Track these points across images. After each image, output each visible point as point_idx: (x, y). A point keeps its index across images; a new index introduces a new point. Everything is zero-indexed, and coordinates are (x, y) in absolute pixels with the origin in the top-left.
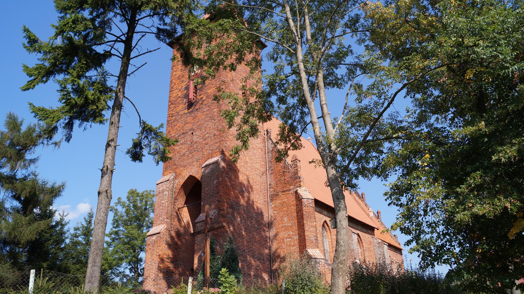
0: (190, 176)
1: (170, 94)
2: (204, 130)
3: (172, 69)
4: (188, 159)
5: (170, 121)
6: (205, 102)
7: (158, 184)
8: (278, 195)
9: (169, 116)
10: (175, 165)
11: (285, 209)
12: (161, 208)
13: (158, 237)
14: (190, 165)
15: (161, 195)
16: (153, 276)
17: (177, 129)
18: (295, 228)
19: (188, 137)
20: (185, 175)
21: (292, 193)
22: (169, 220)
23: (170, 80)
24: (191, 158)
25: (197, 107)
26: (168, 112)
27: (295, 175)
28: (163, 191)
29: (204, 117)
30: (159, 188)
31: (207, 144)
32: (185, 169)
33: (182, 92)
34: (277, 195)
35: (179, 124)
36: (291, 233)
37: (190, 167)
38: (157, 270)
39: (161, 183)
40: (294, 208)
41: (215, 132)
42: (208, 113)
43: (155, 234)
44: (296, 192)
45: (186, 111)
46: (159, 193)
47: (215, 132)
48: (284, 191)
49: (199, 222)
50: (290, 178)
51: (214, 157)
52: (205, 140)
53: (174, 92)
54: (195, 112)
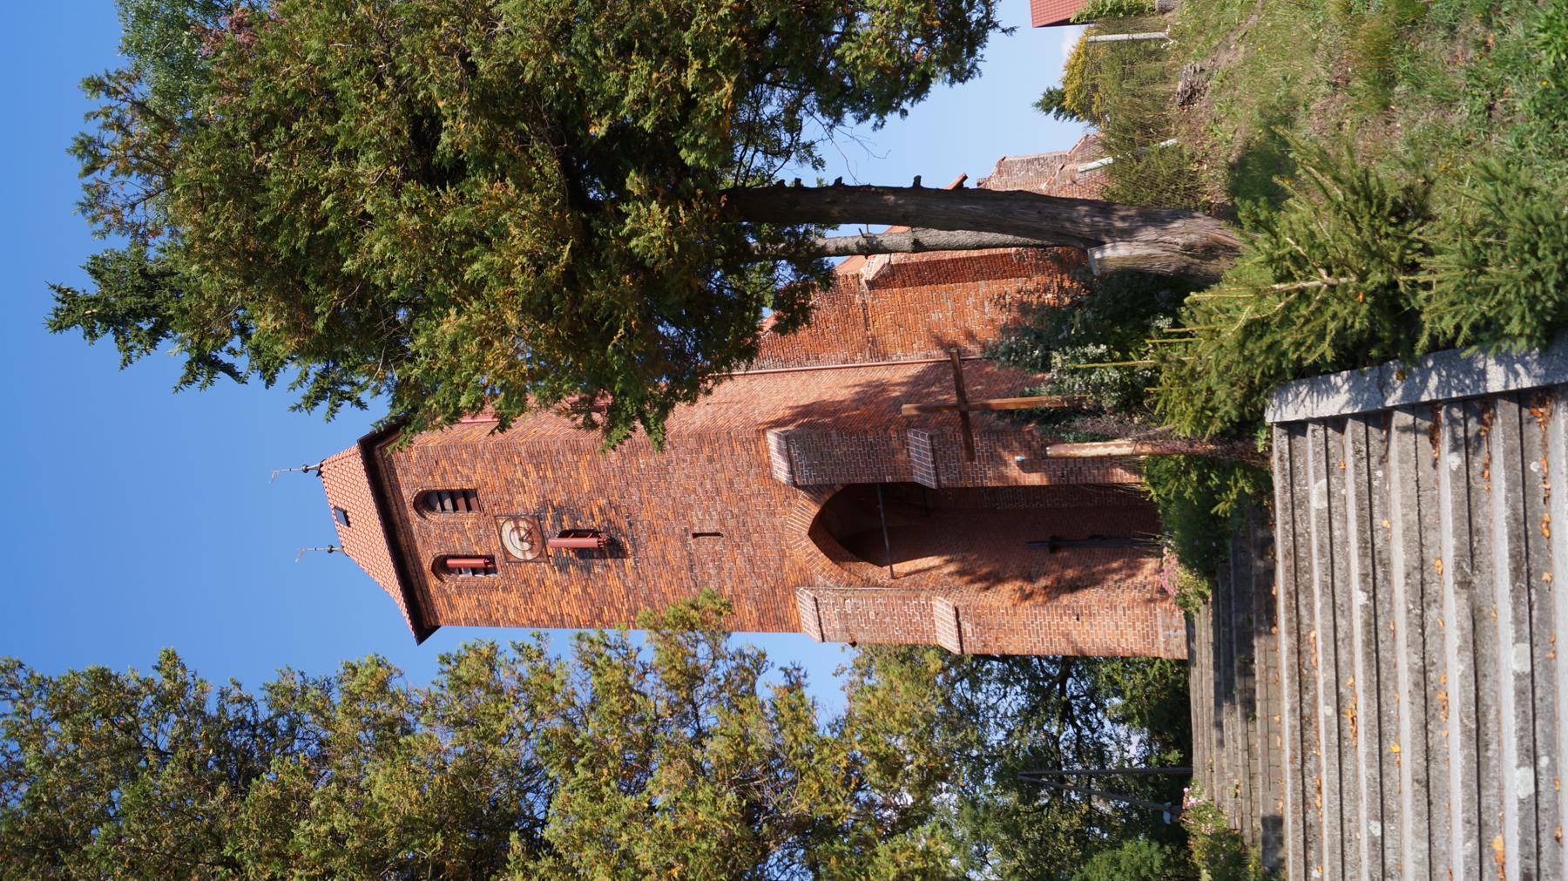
0: (810, 534)
2: (693, 496)
3: (497, 624)
4: (765, 545)
6: (616, 499)
8: (874, 337)
10: (773, 589)
12: (888, 620)
14: (782, 536)
15: (853, 624)
16: (1070, 622)
17: (674, 593)
18: (958, 288)
20: (805, 550)
22: (923, 594)
25: (624, 524)
28: (843, 616)
29: (655, 500)
30: (834, 630)
31: (731, 483)
32: (791, 555)
34: (874, 342)
35: (662, 584)
36: (971, 300)
40: (911, 293)
41: (703, 457)
42: (645, 486)
44: (872, 284)
45: (629, 562)
46: (847, 630)
47: (703, 457)
48: (866, 320)
49: (937, 475)
51: (769, 457)
52: (718, 492)
53: (566, 610)
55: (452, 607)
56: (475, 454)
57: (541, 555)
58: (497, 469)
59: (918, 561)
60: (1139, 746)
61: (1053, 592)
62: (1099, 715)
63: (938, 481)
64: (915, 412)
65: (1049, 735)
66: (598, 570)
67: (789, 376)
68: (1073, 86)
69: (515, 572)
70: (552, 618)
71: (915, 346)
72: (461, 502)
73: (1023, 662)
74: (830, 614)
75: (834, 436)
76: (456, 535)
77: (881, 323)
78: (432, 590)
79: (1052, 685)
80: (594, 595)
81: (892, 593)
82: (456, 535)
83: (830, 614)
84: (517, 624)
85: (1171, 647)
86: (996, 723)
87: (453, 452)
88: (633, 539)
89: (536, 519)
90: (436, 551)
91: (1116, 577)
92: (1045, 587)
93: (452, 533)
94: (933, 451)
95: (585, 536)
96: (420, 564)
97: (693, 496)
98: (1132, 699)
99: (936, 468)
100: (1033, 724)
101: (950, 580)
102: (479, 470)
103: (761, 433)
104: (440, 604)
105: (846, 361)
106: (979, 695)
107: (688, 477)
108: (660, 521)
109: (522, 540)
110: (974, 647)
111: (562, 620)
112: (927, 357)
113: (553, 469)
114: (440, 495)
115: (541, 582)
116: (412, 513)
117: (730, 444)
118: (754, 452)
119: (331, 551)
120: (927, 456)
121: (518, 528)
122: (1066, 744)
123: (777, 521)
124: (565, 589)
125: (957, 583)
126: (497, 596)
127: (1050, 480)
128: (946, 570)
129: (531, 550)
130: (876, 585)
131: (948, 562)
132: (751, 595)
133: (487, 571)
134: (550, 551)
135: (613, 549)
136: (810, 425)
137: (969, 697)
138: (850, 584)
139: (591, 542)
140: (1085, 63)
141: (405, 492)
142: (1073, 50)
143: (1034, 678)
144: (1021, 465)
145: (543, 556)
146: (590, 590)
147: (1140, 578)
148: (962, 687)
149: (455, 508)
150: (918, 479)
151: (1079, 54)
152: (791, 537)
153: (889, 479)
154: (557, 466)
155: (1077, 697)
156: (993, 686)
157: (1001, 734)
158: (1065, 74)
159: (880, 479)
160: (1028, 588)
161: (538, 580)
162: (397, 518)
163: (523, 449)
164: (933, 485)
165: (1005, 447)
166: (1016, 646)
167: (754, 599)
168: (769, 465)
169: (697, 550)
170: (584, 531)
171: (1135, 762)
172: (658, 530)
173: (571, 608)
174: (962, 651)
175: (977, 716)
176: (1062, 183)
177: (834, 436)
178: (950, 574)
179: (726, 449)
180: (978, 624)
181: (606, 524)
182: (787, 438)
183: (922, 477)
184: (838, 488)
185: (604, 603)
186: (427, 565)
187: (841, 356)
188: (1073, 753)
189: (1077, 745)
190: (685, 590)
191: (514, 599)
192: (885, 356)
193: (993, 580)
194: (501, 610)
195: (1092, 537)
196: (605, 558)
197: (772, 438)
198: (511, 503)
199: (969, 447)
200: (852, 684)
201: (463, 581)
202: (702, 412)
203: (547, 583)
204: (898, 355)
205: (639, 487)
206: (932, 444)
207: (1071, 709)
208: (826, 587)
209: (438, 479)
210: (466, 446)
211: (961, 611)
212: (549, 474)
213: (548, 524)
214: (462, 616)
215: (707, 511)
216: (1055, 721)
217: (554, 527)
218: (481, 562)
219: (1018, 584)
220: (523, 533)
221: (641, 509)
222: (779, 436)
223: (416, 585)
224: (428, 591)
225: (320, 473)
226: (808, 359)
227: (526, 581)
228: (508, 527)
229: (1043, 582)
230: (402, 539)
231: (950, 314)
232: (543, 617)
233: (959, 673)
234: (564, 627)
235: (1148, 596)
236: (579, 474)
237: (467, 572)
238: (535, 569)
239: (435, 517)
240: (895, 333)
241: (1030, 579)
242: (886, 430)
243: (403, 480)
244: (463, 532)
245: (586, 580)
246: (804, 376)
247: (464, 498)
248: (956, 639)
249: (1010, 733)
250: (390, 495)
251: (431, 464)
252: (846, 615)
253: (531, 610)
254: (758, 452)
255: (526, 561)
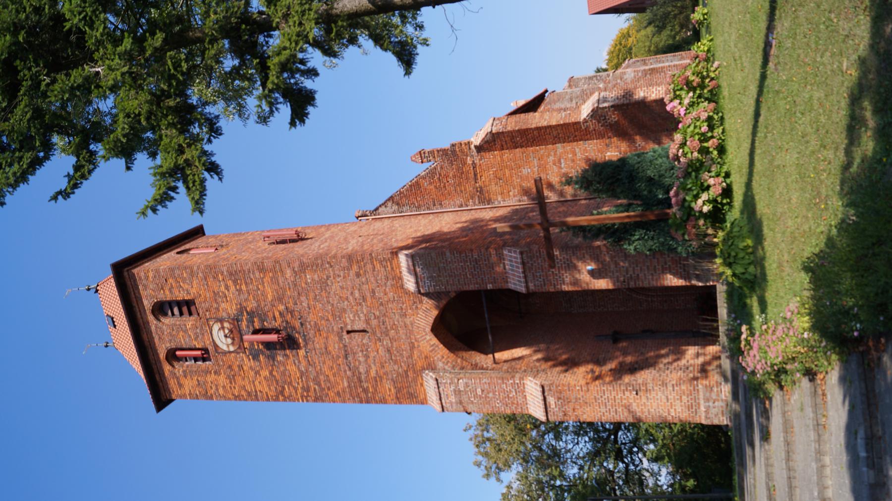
1: (262, 399)
2: (346, 303)
3: (211, 398)
5: (316, 394)
6: (291, 305)
7: (442, 407)
9: (306, 397)
10: (406, 372)
11: (507, 172)
12: (491, 395)
13: (550, 390)
14: (411, 332)
15: (465, 398)
16: (630, 396)
17: (334, 375)
18: (542, 150)
19: (354, 343)
20: (429, 342)
21: (480, 160)
22: (517, 375)
23: (233, 402)
24: (397, 333)
25: (297, 324)
26: (298, 401)
27: (447, 154)
28: (457, 392)
30: (451, 403)
31: (373, 292)
32: (419, 346)
33: (262, 368)
34: (481, 192)
35: (326, 369)
36: (551, 158)
37: (415, 330)
38: (617, 387)
39: (440, 399)
41: (352, 273)
42: (312, 295)
43: (545, 399)
44: (479, 149)
45: (302, 352)
46: (461, 403)
47: (352, 273)
48: (475, 175)
49: (526, 282)
50: (452, 165)
51: (401, 272)
52: (364, 299)
53: (259, 388)
54: (306, 328)
55: (181, 386)
56: (192, 274)
57: (239, 347)
58: (207, 284)
59: (514, 351)
60: (666, 476)
61: (619, 372)
62: (640, 455)
63: (527, 287)
64: (507, 229)
65: (609, 471)
66: (280, 358)
67: (420, 217)
68: (613, 64)
69: (222, 360)
70: (249, 394)
71: (511, 193)
72: (185, 309)
73: (591, 424)
74: (448, 390)
75: (448, 254)
76: (181, 333)
77: (486, 177)
78: (167, 373)
79: (609, 436)
80: (278, 377)
81: (494, 374)
82: (181, 333)
83: (448, 390)
84: (225, 398)
85: (710, 415)
86: (572, 461)
87: (177, 272)
88: (304, 335)
89: (236, 321)
90: (168, 345)
91: (665, 361)
92: (611, 370)
93: (178, 332)
94: (523, 263)
95: (270, 333)
96: (158, 355)
97: (346, 303)
98: (664, 446)
99: (525, 277)
100: (597, 463)
101: (538, 364)
102: (195, 286)
103: (395, 253)
104: (172, 384)
105: (461, 206)
106: (561, 443)
107: (342, 288)
108: (323, 322)
109: (226, 336)
110: (556, 416)
111: (256, 396)
112: (520, 201)
113: (246, 284)
114: (171, 304)
115: (241, 367)
116: (151, 318)
117: (372, 263)
118: (389, 268)
119: (107, 346)
120: (517, 267)
121: (223, 328)
122: (618, 475)
123: (408, 321)
124: (257, 373)
125: (543, 367)
126: (211, 378)
127: (614, 285)
128: (535, 358)
129: (233, 344)
130: (482, 368)
131: (536, 352)
132: (390, 376)
133: (204, 360)
134: (246, 345)
135: (290, 343)
136: (434, 248)
137: (554, 444)
138: (462, 368)
139: (273, 337)
140: (620, 50)
141: (145, 302)
142: (612, 42)
143: (596, 431)
144: (592, 273)
145: (241, 348)
146: (275, 373)
147: (683, 362)
148: (549, 438)
149: (181, 314)
150: (512, 286)
151: (616, 45)
152: (418, 333)
153: (490, 287)
154: (249, 281)
155: (625, 444)
156: (569, 437)
157: (575, 470)
158: (607, 57)
159: (483, 287)
160: (597, 370)
161: (239, 366)
162: (141, 321)
163: (225, 269)
164: (523, 290)
165: (579, 259)
166: (589, 414)
167: (392, 380)
168: (401, 278)
169: (350, 343)
170: (268, 329)
171: (665, 487)
172: (321, 328)
173: (262, 386)
174: (548, 419)
175: (559, 458)
176: (614, 82)
177: (448, 254)
178: (538, 360)
179: (369, 267)
180: (559, 398)
181: (284, 324)
182: (412, 257)
183: (515, 284)
184: (453, 295)
185: (285, 382)
186: (162, 355)
187: (458, 202)
188: (623, 480)
189: (626, 476)
190: (342, 374)
191: (222, 380)
192: (489, 202)
193: (570, 364)
194: (214, 388)
195: (644, 331)
196: (285, 349)
197: (402, 258)
198: (217, 309)
199: (551, 257)
200: (476, 436)
201: (188, 366)
202: (355, 241)
203: (245, 368)
204: (499, 200)
205: (307, 296)
206: (522, 258)
207: (622, 452)
208: (445, 370)
209: (167, 292)
210: (186, 268)
211: (546, 388)
212: (244, 287)
213: (244, 324)
214: (187, 392)
215: (356, 314)
216: (611, 460)
217: (248, 327)
218: (199, 353)
219: (590, 367)
220: (227, 331)
221: (309, 313)
222: (407, 255)
223: (155, 370)
224: (164, 374)
225: (97, 291)
226: (434, 205)
227: (230, 367)
228: (216, 327)
229: (612, 365)
230: (145, 336)
231: (536, 169)
232: (243, 393)
233: (546, 429)
234: (258, 400)
235: (691, 375)
236: (264, 287)
237: (191, 360)
238: (236, 358)
239: (167, 321)
240: (496, 184)
241: (599, 362)
242: (487, 249)
243: (143, 293)
244: (186, 331)
245: (272, 366)
246: (431, 217)
247: (187, 306)
248: (542, 409)
249: (581, 468)
250: (135, 304)
251: (162, 282)
252: (460, 391)
253: (235, 388)
254: (392, 268)
255: (230, 352)
